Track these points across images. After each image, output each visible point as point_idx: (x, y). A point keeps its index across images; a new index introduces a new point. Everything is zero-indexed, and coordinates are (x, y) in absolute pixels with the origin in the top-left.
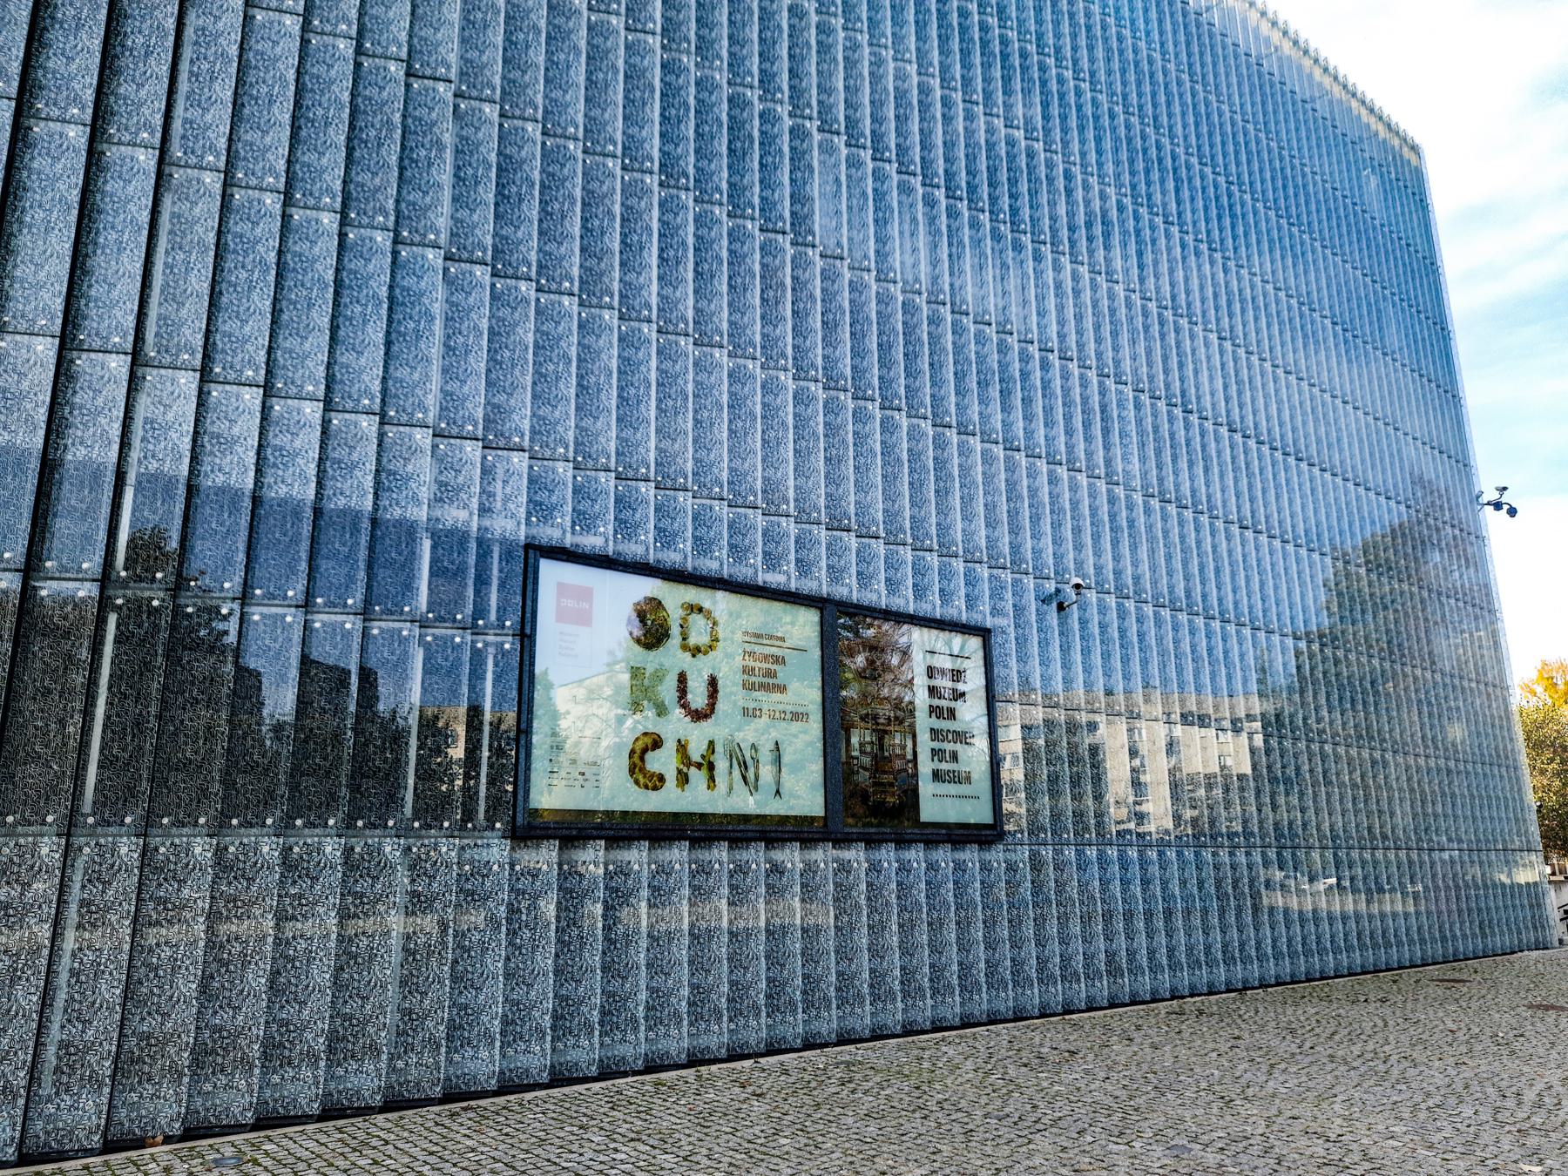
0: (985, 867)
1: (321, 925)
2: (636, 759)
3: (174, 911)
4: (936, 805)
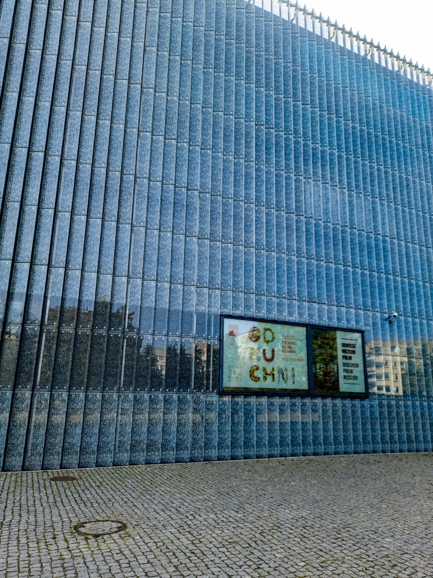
0: (363, 406)
1: (173, 416)
2: (252, 373)
3: (141, 411)
4: (344, 386)
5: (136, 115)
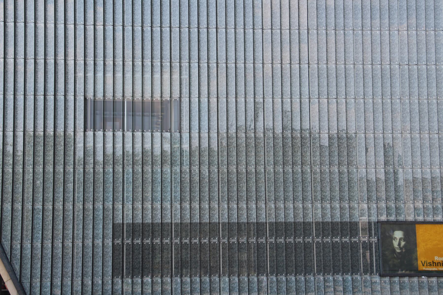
5: (352, 88)
